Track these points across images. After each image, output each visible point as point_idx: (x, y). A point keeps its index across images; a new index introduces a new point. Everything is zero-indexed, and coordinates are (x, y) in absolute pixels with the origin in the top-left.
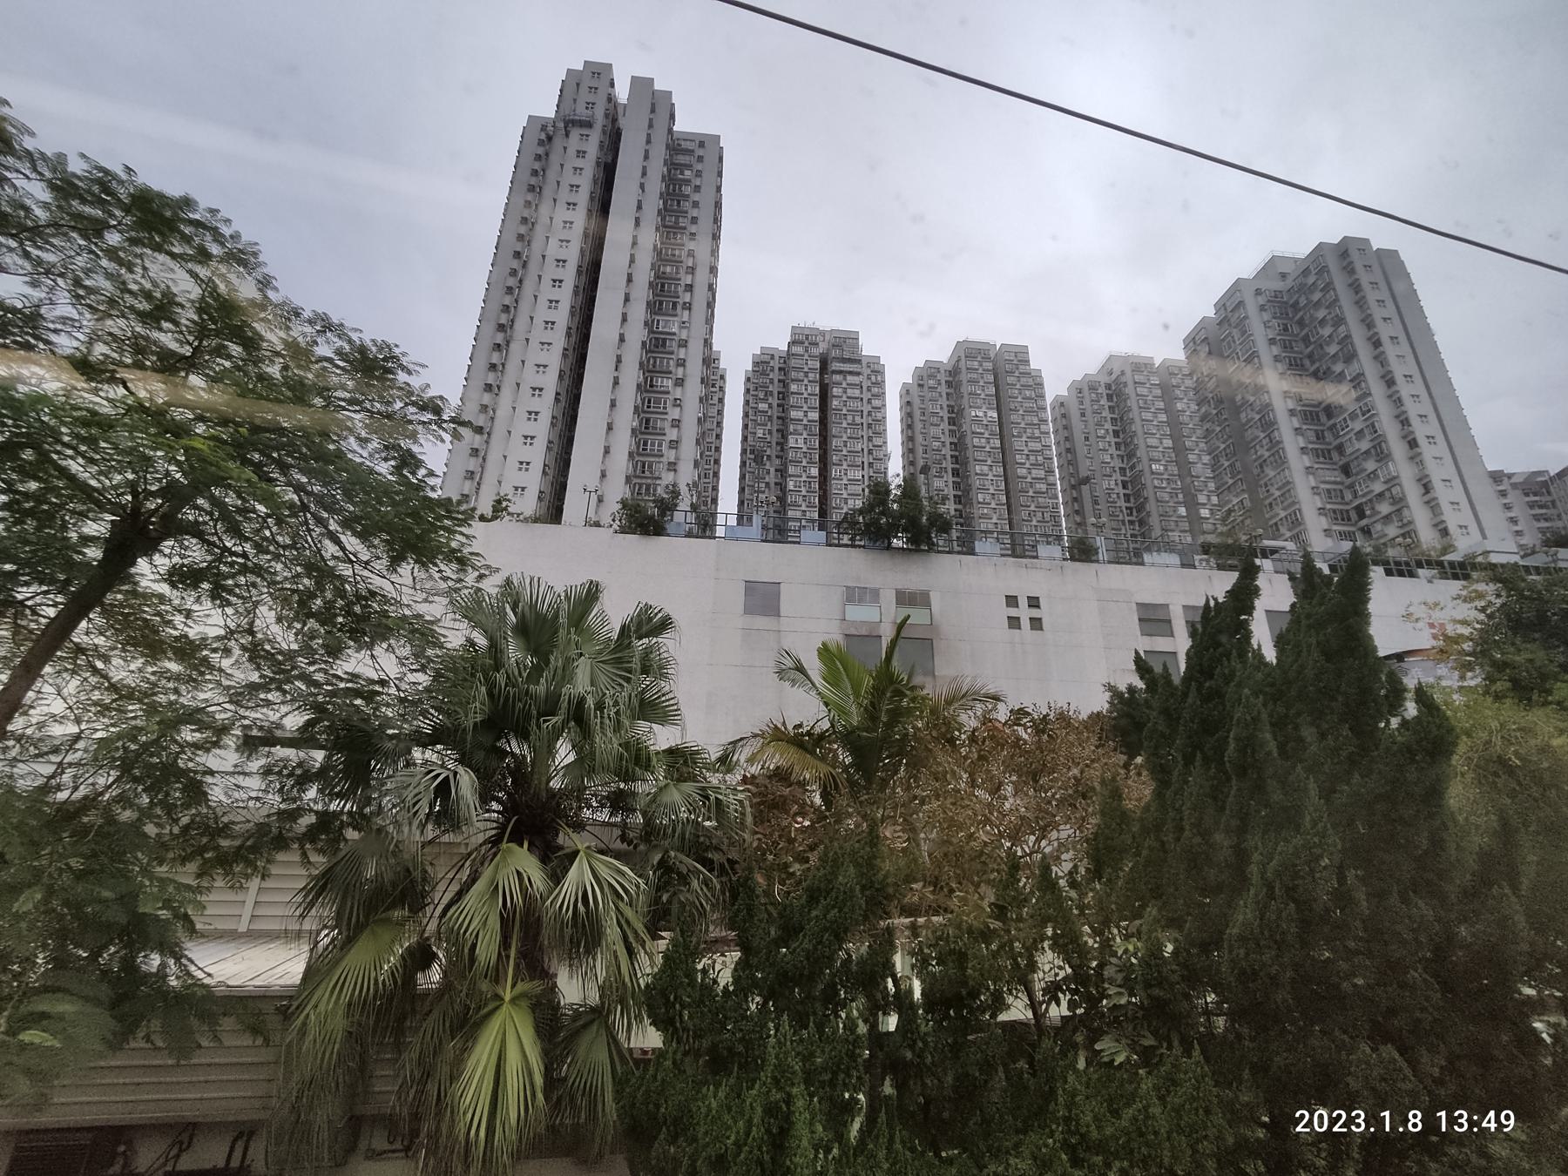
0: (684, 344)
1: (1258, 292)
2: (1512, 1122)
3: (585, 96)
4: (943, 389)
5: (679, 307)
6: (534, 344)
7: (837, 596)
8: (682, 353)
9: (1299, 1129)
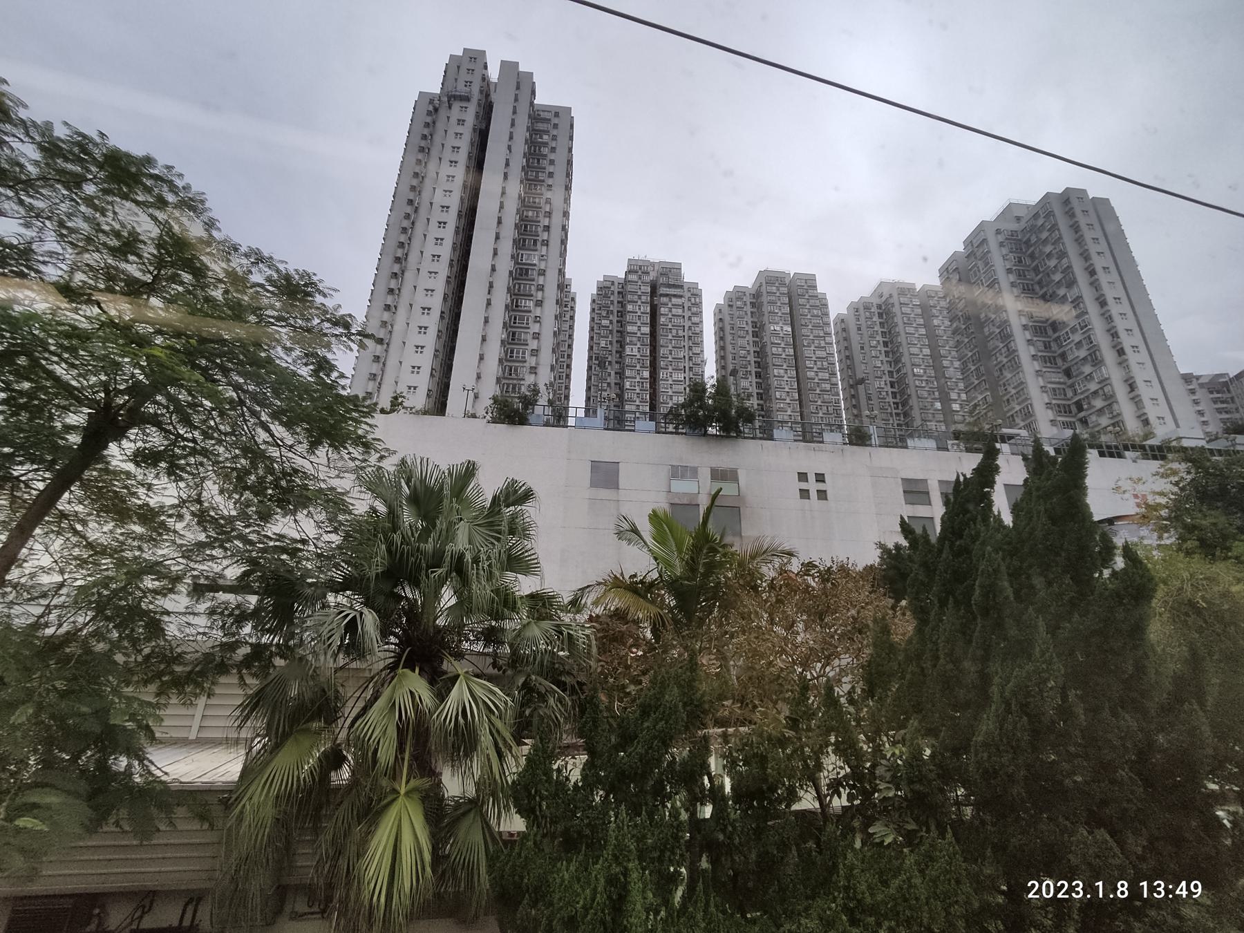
0: (542, 273)
1: (998, 232)
2: (1200, 890)
3: (464, 76)
4: (748, 309)
5: (539, 244)
6: (424, 273)
7: (664, 472)
8: (541, 280)
9: (1030, 896)
